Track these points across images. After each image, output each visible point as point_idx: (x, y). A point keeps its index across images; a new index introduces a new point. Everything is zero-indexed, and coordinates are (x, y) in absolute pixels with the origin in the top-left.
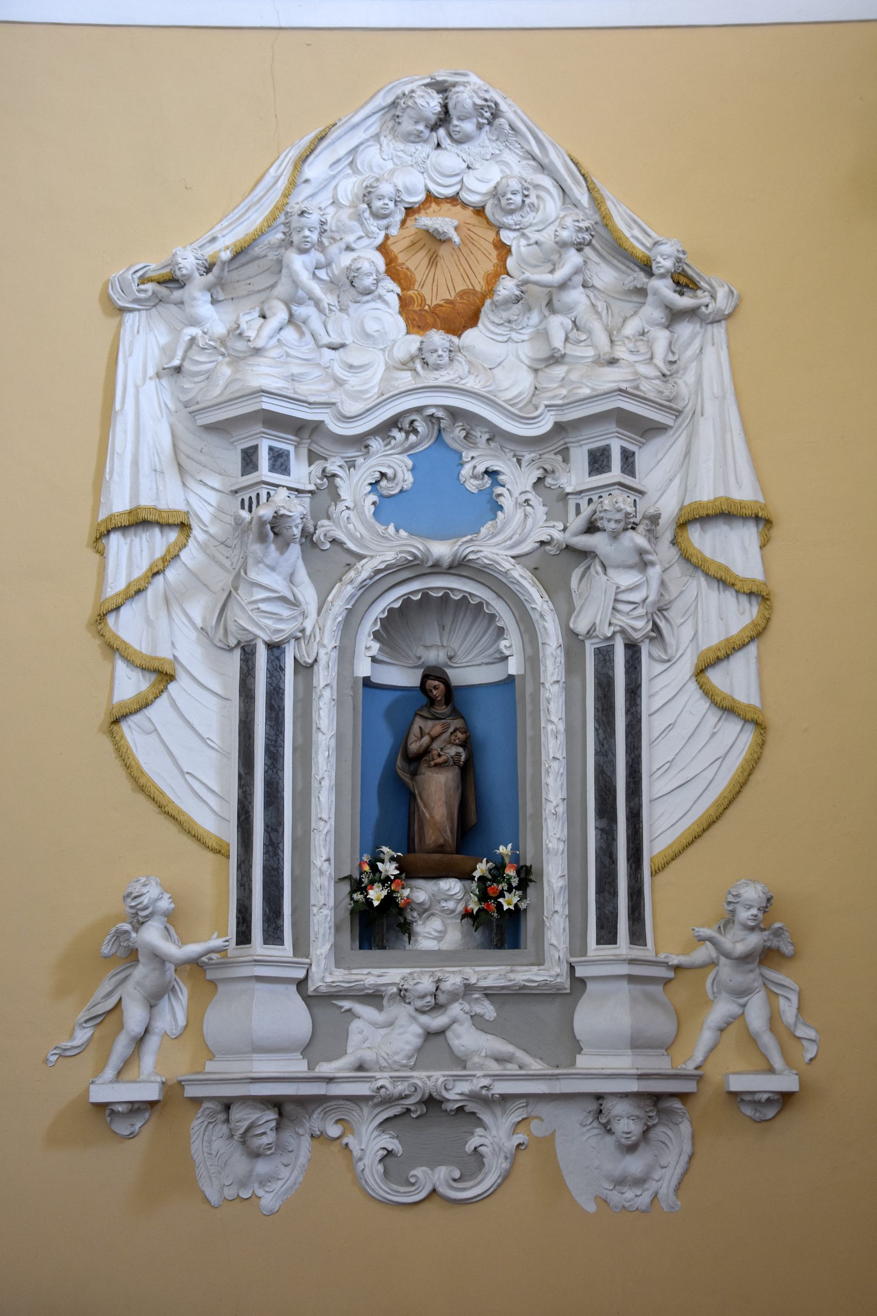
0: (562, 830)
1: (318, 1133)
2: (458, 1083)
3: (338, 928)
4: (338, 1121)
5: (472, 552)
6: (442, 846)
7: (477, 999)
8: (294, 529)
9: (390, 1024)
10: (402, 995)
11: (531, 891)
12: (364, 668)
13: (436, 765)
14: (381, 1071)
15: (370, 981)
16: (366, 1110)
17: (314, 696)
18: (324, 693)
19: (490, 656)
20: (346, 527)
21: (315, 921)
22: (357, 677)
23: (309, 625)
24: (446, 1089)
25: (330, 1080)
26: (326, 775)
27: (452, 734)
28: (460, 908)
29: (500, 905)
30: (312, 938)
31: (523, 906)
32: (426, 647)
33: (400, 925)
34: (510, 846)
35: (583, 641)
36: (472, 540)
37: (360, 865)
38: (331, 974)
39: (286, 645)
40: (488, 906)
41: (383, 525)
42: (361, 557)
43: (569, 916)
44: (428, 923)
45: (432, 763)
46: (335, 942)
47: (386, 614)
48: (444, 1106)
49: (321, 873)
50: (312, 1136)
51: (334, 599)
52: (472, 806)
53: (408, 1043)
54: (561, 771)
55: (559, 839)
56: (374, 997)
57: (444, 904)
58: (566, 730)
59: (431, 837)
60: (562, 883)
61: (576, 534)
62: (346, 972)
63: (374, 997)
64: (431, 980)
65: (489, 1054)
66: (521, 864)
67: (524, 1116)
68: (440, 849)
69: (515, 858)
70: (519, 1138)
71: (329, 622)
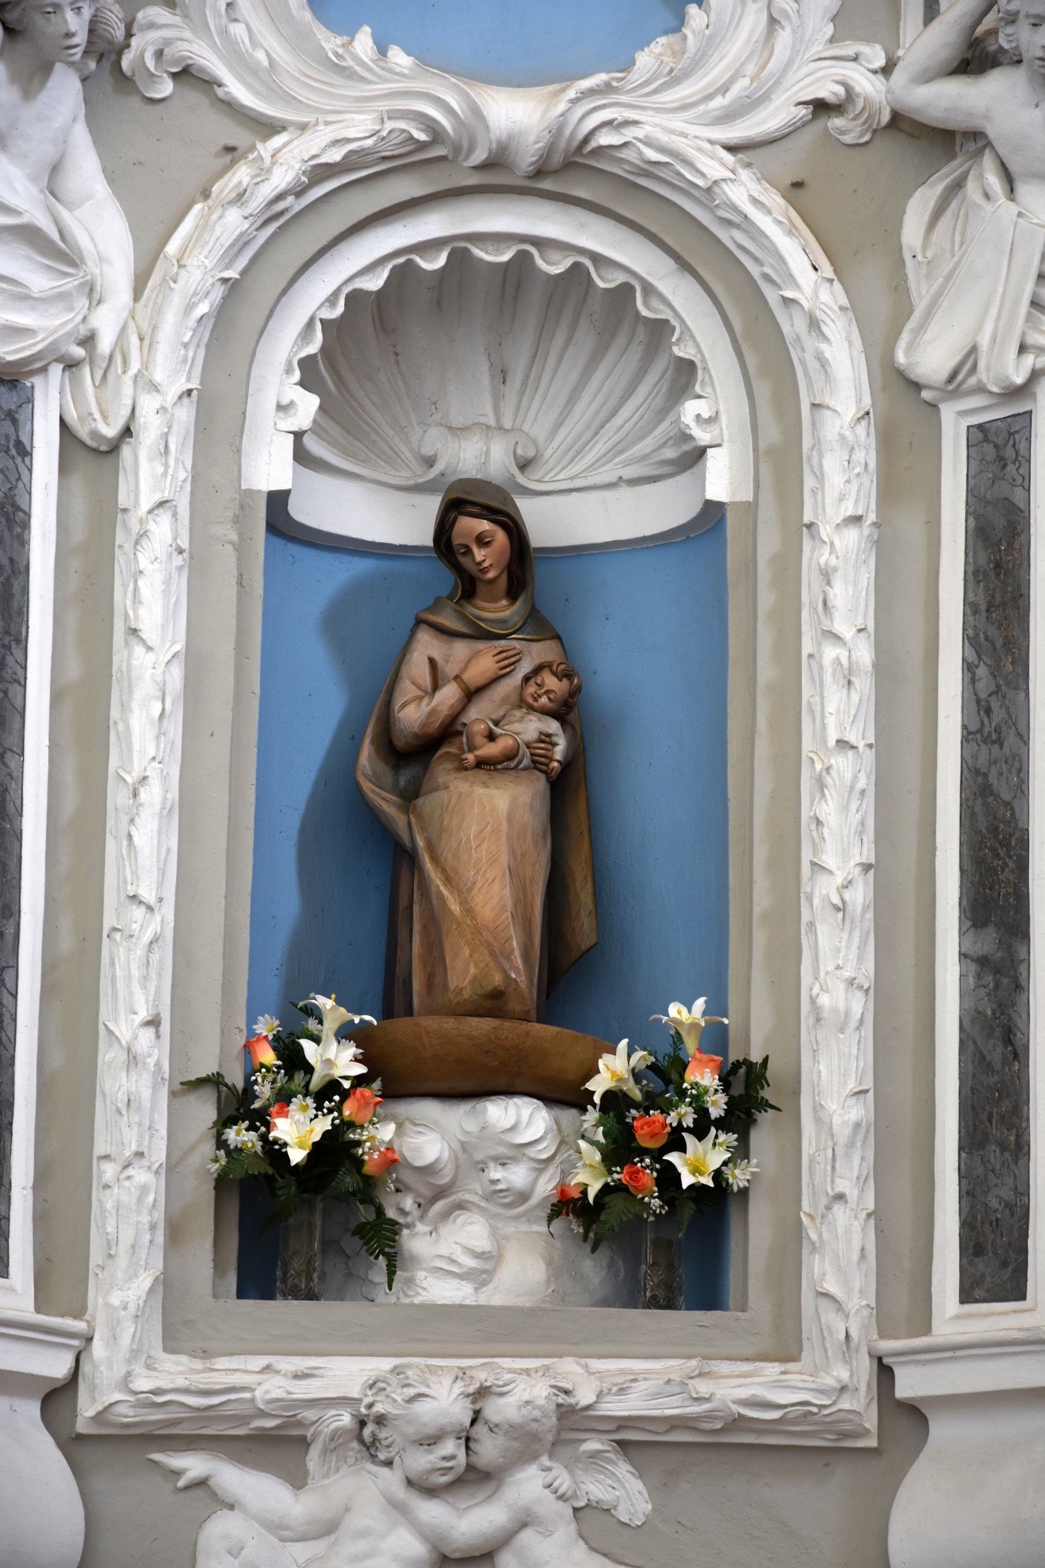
0: (860, 959)
3: (175, 1232)
5: (608, 124)
6: (497, 995)
7: (594, 1455)
8: (70, 15)
9: (327, 1529)
10: (367, 1436)
11: (763, 1136)
12: (270, 468)
13: (481, 764)
15: (272, 1389)
17: (120, 538)
18: (152, 526)
19: (643, 458)
20: (224, 33)
21: (109, 1205)
22: (251, 493)
23: (107, 322)
26: (153, 771)
27: (527, 679)
28: (546, 1187)
29: (669, 1176)
30: (96, 1257)
31: (738, 1177)
32: (451, 429)
33: (362, 1231)
34: (700, 1003)
35: (933, 406)
36: (608, 88)
37: (248, 1049)
38: (149, 1367)
39: (37, 381)
40: (634, 1175)
41: (339, 33)
42: (269, 128)
43: (877, 1215)
44: (445, 1230)
45: (470, 757)
46: (165, 1272)
47: (340, 308)
49: (133, 1060)
51: (184, 250)
52: (583, 896)
54: (862, 783)
55: (851, 982)
56: (278, 1443)
57: (496, 1173)
58: (877, 666)
59: (465, 971)
60: (858, 1112)
61: (927, 77)
62: (198, 1364)
63: (278, 1443)
64: (459, 1388)
66: (734, 1056)
68: (493, 1003)
69: (716, 1039)
71: (170, 318)
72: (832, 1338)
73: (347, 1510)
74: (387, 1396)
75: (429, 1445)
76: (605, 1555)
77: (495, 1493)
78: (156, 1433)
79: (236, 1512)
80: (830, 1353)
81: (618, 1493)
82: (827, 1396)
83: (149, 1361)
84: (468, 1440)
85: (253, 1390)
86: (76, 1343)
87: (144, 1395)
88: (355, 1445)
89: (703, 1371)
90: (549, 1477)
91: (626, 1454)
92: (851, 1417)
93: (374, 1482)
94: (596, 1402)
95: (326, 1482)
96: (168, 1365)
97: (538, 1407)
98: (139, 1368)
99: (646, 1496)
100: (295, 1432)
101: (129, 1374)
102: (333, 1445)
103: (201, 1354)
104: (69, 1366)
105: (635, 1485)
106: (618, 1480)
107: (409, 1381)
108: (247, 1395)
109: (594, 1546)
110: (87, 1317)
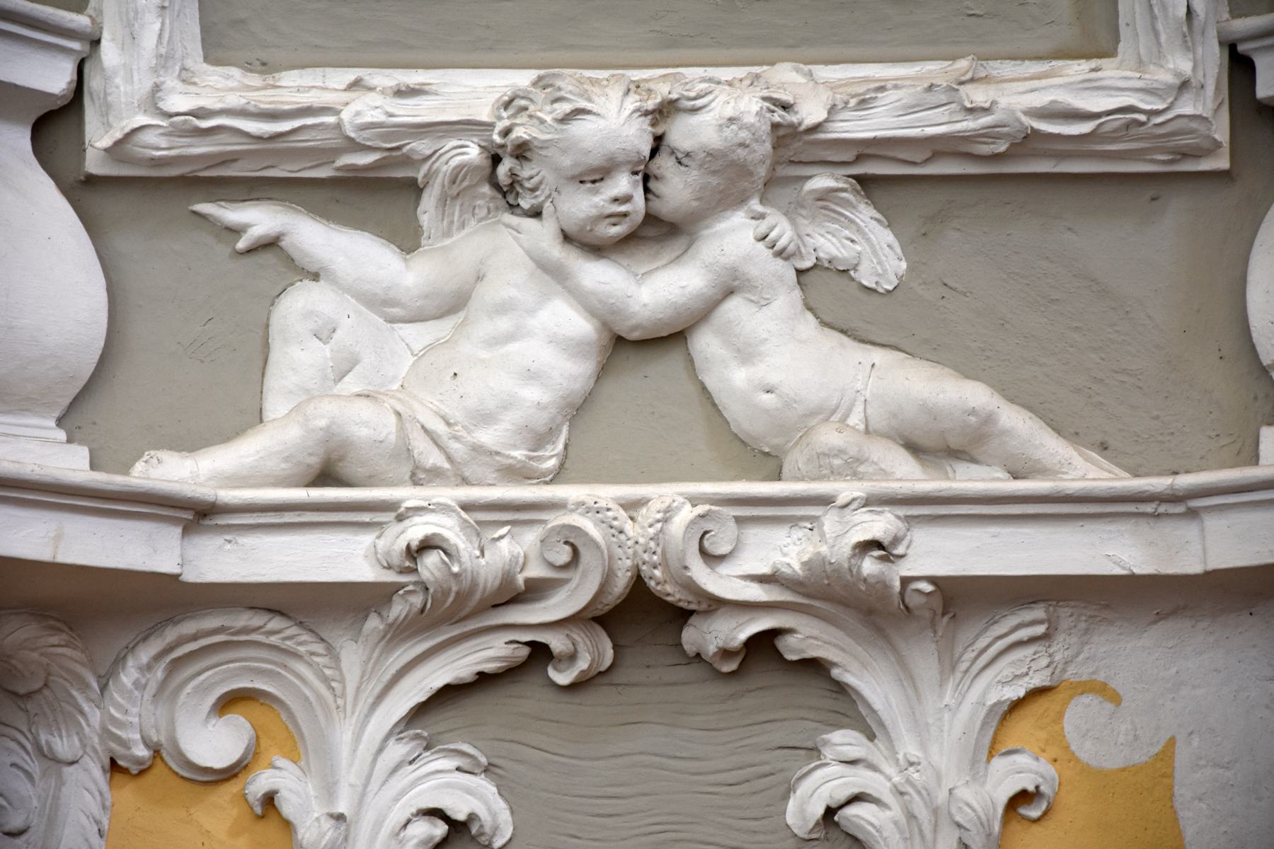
1: (141, 752)
2: (755, 534)
4: (229, 702)
7: (825, 196)
9: (452, 304)
14: (416, 482)
16: (352, 655)
24: (703, 552)
25: (198, 515)
48: (691, 637)
50: (114, 767)
53: (531, 375)
56: (378, 189)
62: (255, 80)
64: (632, 103)
65: (877, 422)
67: (1037, 681)
70: (1012, 773)
72: (1166, 17)
73: (479, 278)
74: (531, 116)
75: (594, 182)
76: (843, 331)
77: (686, 251)
78: (202, 174)
79: (322, 282)
80: (1163, 38)
81: (858, 248)
82: (1160, 96)
83: (184, 75)
84: (646, 179)
85: (337, 112)
86: (76, 45)
87: (182, 118)
88: (486, 189)
89: (977, 76)
90: (763, 227)
91: (868, 196)
92: (1194, 125)
93: (515, 239)
94: (826, 121)
95: (447, 242)
96: (212, 78)
97: (748, 127)
98: (170, 81)
99: (899, 250)
100: (399, 174)
101: (157, 88)
102: (455, 190)
103: (260, 68)
104: (68, 79)
105: (884, 237)
106: (859, 230)
107: (562, 94)
108: (330, 119)
109: (828, 319)
110: (90, 11)
